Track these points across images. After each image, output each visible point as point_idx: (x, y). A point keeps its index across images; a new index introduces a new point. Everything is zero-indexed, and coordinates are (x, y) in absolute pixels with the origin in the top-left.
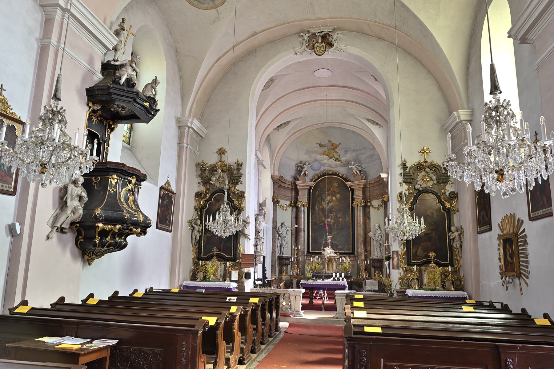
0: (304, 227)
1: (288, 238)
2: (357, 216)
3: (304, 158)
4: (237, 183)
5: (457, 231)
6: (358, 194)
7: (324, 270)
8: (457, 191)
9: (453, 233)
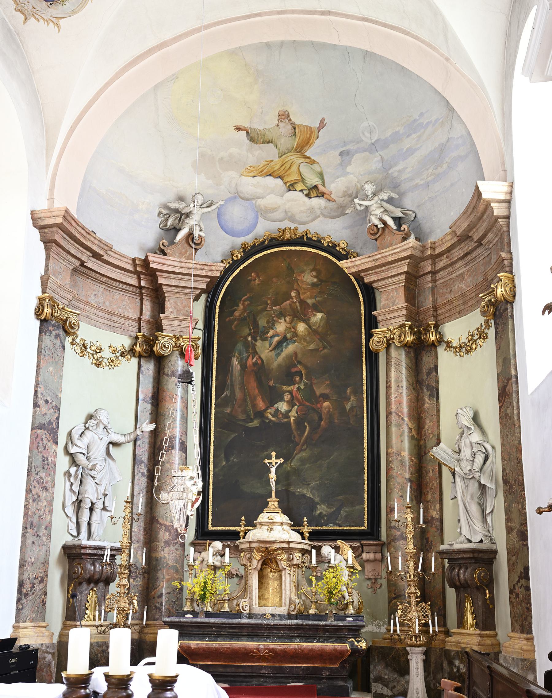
2: (388, 387)
3: (191, 182)
6: (392, 307)
7: (244, 603)
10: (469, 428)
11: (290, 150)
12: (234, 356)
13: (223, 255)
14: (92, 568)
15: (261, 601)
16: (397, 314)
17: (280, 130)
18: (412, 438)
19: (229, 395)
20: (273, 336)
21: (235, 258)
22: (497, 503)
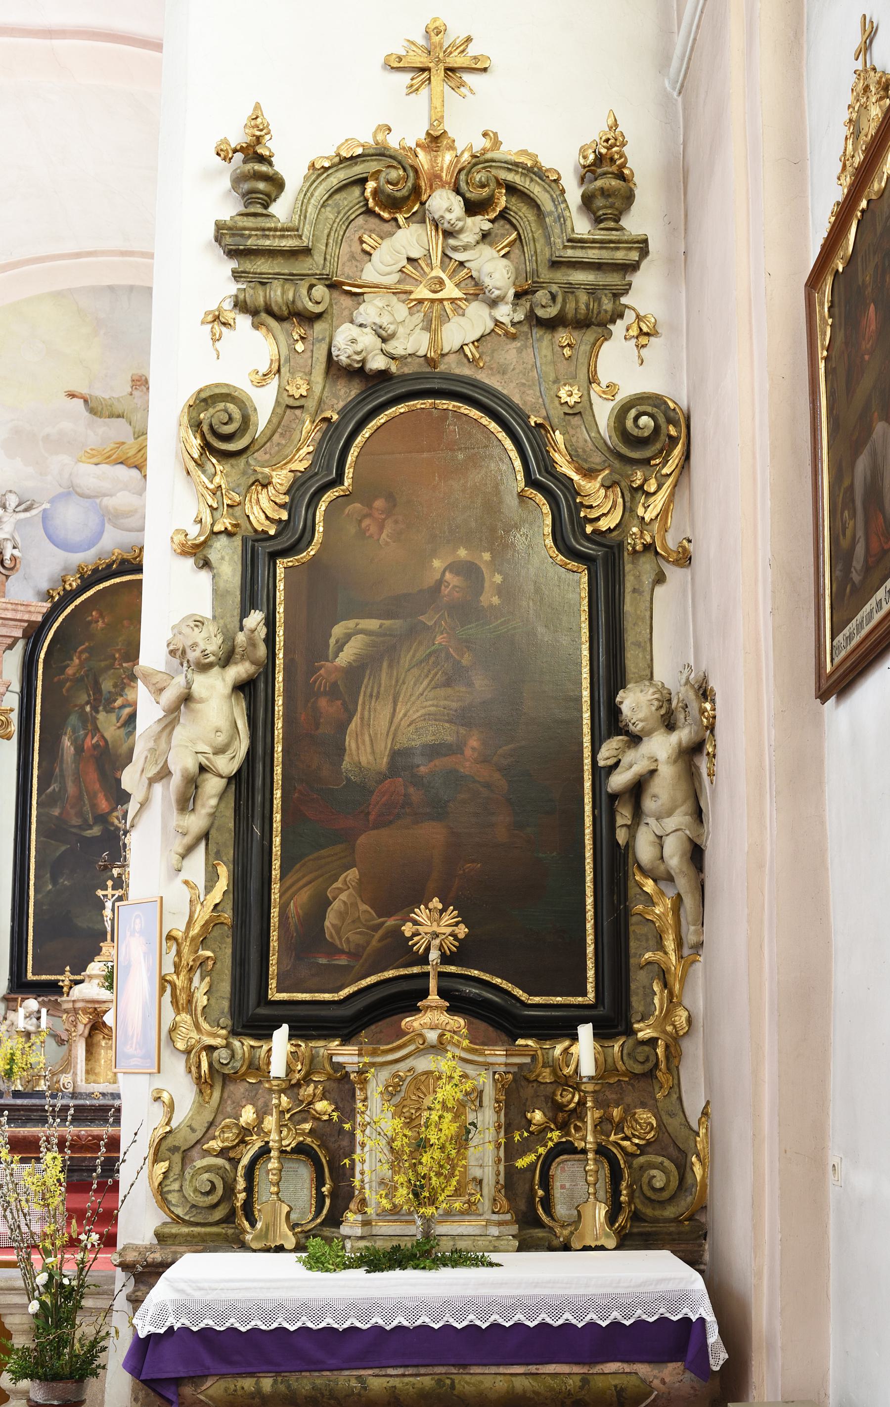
5: (669, 724)
7: (65, 1079)
8: (679, 395)
9: (635, 740)
12: (66, 734)
13: (51, 580)
14: (325, 394)
15: (90, 1076)
17: (135, 401)
19: (57, 789)
20: (122, 707)
21: (68, 588)
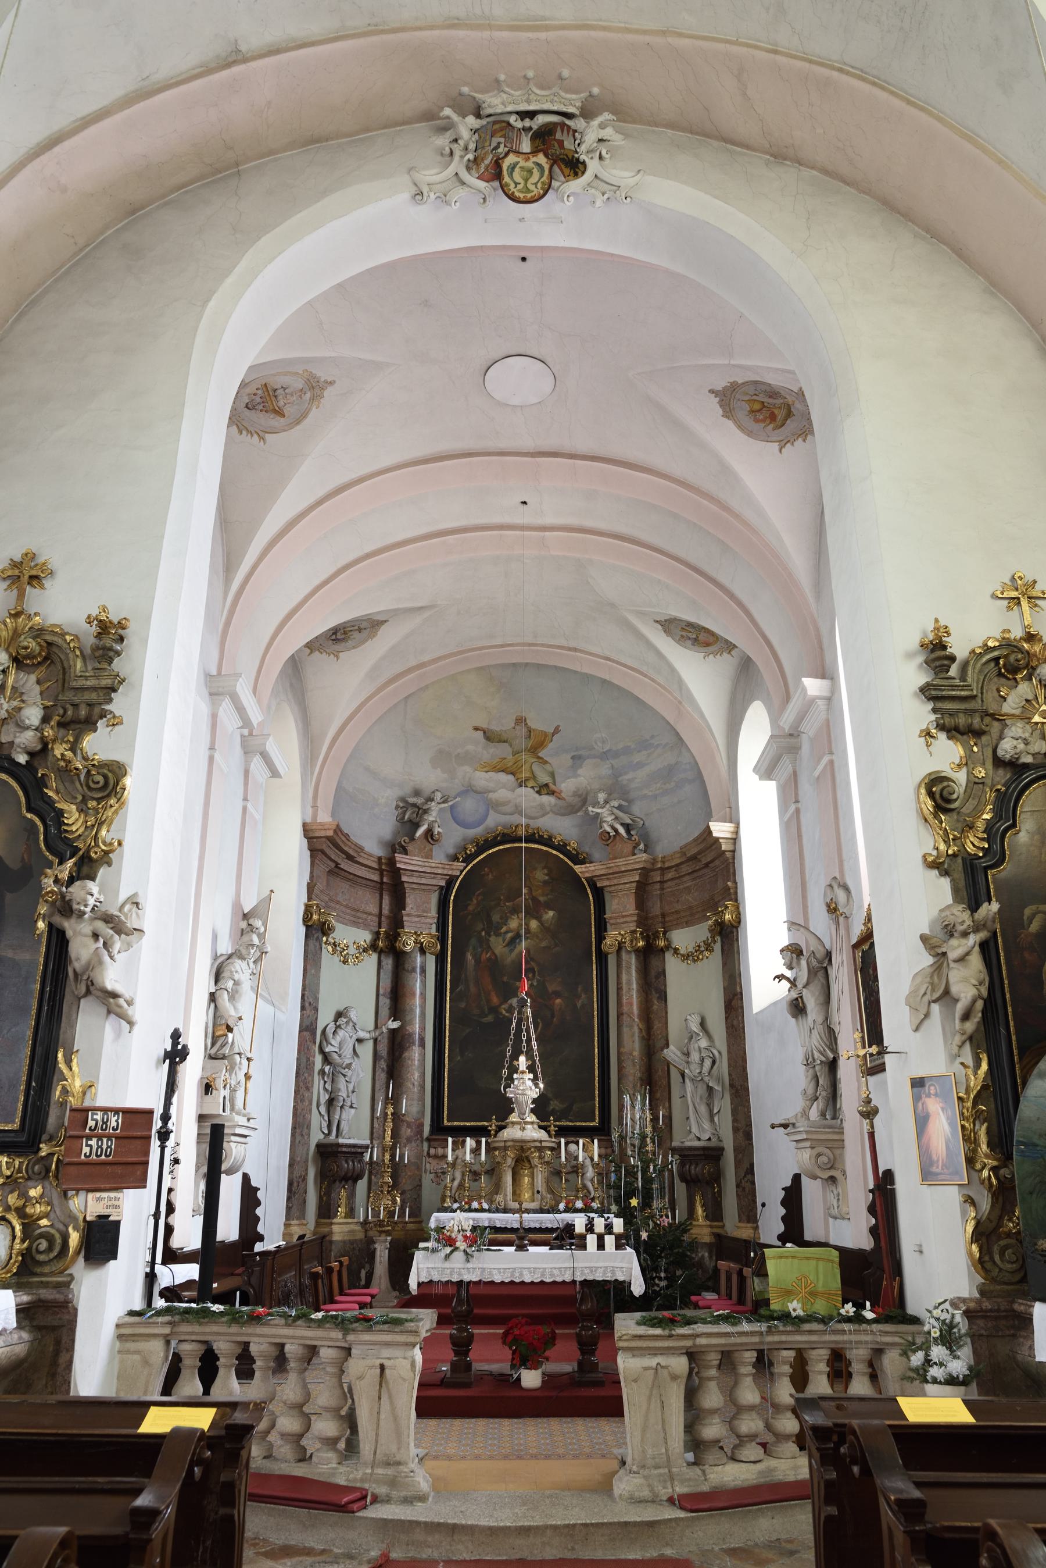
0: (423, 1028)
1: (361, 1072)
2: (619, 989)
3: (429, 777)
4: (89, 724)
6: (621, 907)
10: (698, 1035)
11: (522, 749)
16: (628, 919)
18: (642, 1038)
20: (506, 932)
22: (724, 1104)
